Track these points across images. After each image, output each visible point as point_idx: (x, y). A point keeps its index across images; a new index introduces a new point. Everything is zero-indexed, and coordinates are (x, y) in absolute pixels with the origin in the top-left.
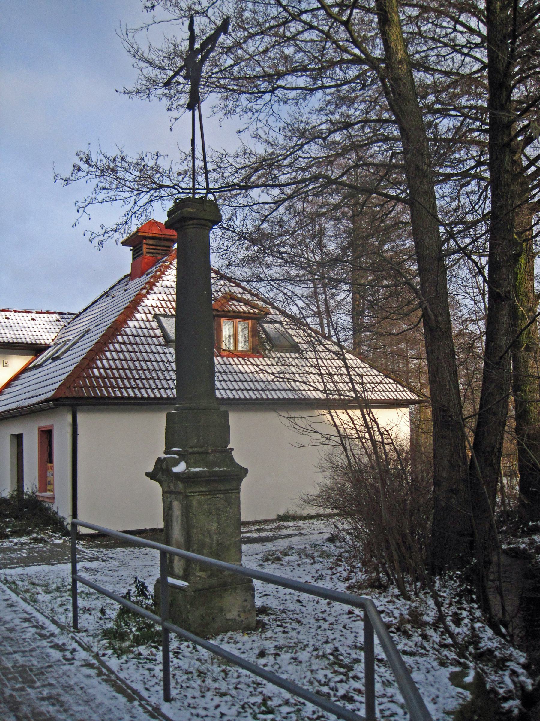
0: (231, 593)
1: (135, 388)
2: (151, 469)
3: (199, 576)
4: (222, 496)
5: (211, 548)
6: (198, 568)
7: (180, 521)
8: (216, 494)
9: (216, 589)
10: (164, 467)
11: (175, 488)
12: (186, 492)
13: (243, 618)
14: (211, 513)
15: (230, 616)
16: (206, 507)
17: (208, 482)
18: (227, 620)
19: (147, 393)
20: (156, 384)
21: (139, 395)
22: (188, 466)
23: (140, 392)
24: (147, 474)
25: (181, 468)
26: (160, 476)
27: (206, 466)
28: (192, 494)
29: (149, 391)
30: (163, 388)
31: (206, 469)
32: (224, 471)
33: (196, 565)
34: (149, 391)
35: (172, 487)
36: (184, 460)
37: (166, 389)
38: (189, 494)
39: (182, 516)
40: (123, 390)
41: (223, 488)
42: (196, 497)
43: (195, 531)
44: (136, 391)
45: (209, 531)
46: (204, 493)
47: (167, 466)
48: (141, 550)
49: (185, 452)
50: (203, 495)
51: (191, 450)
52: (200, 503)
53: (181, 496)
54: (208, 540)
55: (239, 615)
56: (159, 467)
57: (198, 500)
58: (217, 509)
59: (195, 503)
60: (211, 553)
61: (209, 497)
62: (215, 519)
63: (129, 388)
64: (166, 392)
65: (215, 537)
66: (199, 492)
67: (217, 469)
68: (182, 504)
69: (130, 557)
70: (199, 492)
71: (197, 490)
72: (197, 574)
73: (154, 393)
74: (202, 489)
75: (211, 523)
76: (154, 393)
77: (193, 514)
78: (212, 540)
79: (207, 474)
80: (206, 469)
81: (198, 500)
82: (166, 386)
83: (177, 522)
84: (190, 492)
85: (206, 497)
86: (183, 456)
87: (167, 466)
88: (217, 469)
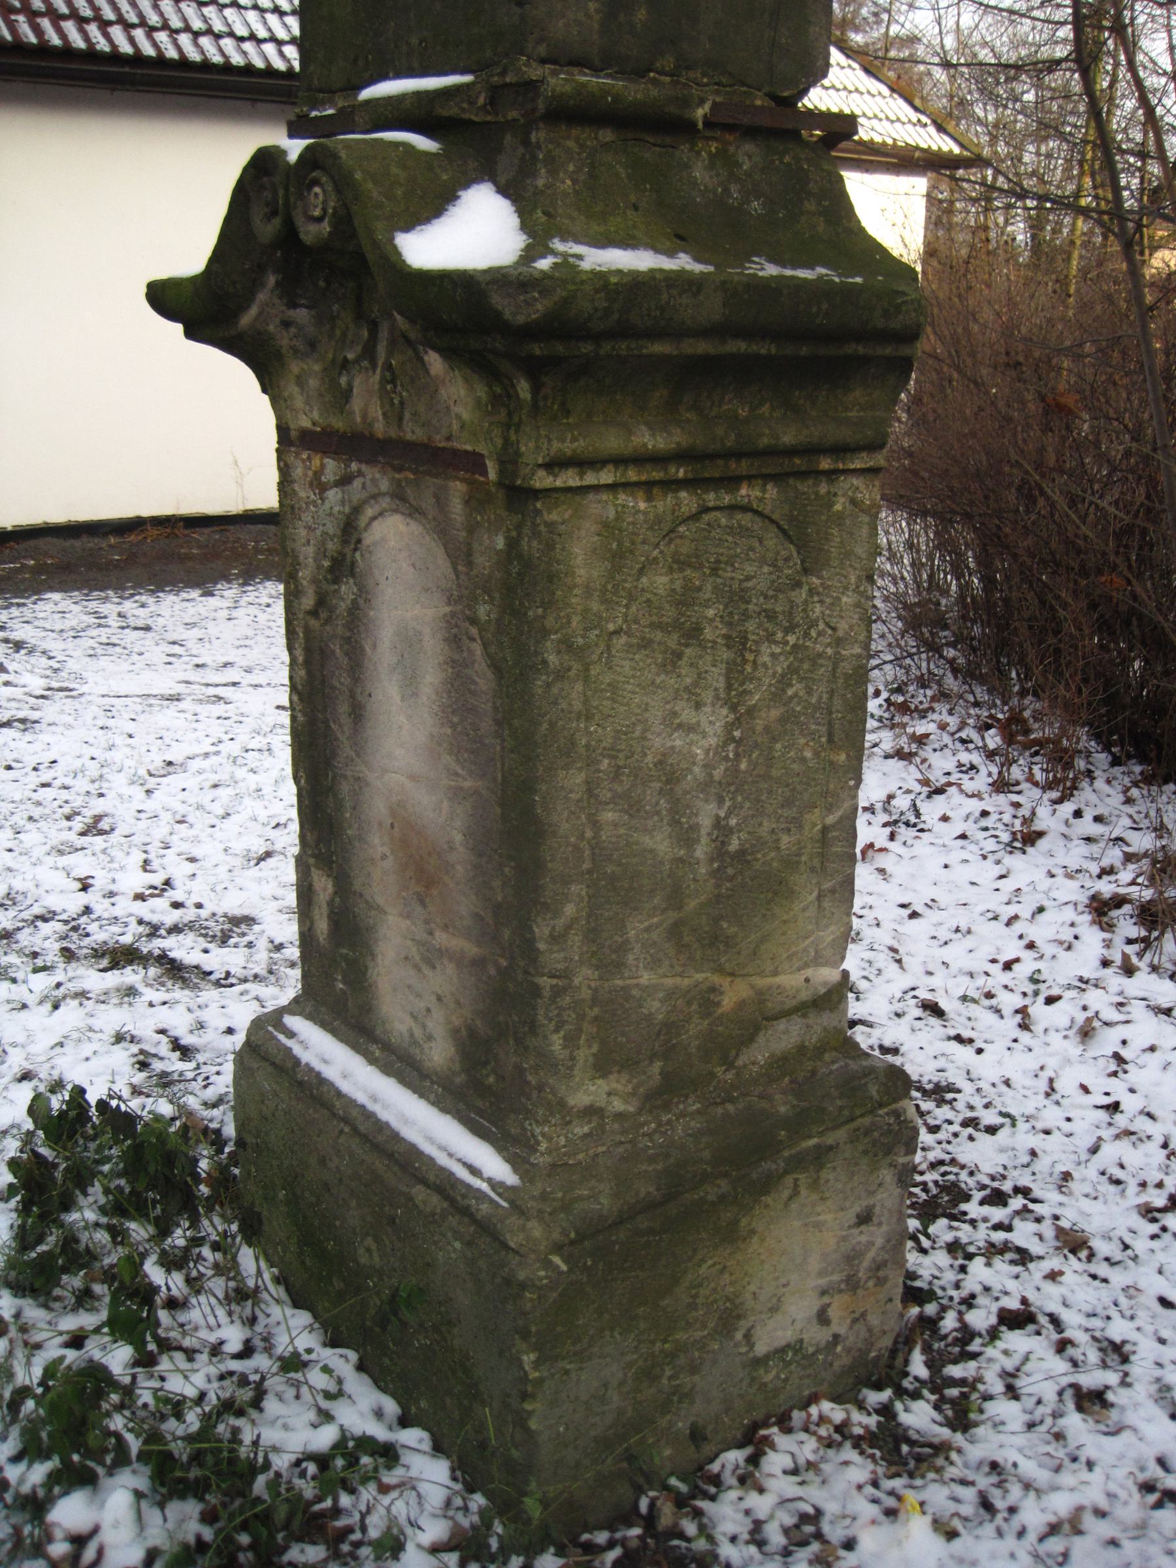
0: (796, 1193)
1: (86, 20)
2: (190, 252)
3: (591, 1111)
4: (772, 491)
5: (676, 898)
6: (585, 1054)
7: (431, 678)
8: (731, 482)
9: (711, 1192)
10: (312, 232)
11: (396, 415)
12: (509, 460)
13: (839, 1325)
14: (693, 634)
15: (770, 1335)
16: (660, 582)
17: (694, 377)
18: (760, 1362)
19: (132, 41)
20: (161, 14)
21: (103, 45)
22: (538, 223)
23: (107, 36)
24: (164, 297)
25: (474, 234)
26: (261, 309)
27: (678, 241)
28: (569, 478)
29: (139, 34)
30: (187, 29)
31: (683, 262)
32: (820, 289)
33: (571, 1041)
34: (139, 34)
35: (367, 406)
36: (486, 172)
37: (196, 35)
38: (543, 480)
39: (454, 641)
40: (45, 23)
41: (788, 437)
42: (602, 507)
43: (574, 779)
44: (93, 29)
45: (669, 774)
46: (652, 472)
47: (344, 222)
48: (128, 606)
49: (496, 94)
50: (648, 487)
51: (560, 82)
52: (617, 551)
53: (457, 489)
54: (660, 842)
55: (823, 1318)
56: (267, 230)
57: (608, 528)
58: (736, 597)
59: (581, 558)
60: (675, 931)
61: (687, 501)
62: (717, 678)
63: (64, 17)
64: (196, 45)
65: (706, 814)
66: (620, 461)
67: (772, 270)
68: (461, 555)
69: (85, 643)
70: (620, 461)
71: (612, 442)
72: (579, 1100)
73: (155, 45)
74: (648, 439)
75: (687, 714)
76: (155, 45)
77: (567, 645)
78: (687, 837)
79: (712, 309)
80: (683, 262)
81: (608, 528)
82: (197, 25)
83: (410, 684)
84: (554, 465)
85: (664, 504)
86: (473, 143)
87: (344, 222)
88: (772, 270)
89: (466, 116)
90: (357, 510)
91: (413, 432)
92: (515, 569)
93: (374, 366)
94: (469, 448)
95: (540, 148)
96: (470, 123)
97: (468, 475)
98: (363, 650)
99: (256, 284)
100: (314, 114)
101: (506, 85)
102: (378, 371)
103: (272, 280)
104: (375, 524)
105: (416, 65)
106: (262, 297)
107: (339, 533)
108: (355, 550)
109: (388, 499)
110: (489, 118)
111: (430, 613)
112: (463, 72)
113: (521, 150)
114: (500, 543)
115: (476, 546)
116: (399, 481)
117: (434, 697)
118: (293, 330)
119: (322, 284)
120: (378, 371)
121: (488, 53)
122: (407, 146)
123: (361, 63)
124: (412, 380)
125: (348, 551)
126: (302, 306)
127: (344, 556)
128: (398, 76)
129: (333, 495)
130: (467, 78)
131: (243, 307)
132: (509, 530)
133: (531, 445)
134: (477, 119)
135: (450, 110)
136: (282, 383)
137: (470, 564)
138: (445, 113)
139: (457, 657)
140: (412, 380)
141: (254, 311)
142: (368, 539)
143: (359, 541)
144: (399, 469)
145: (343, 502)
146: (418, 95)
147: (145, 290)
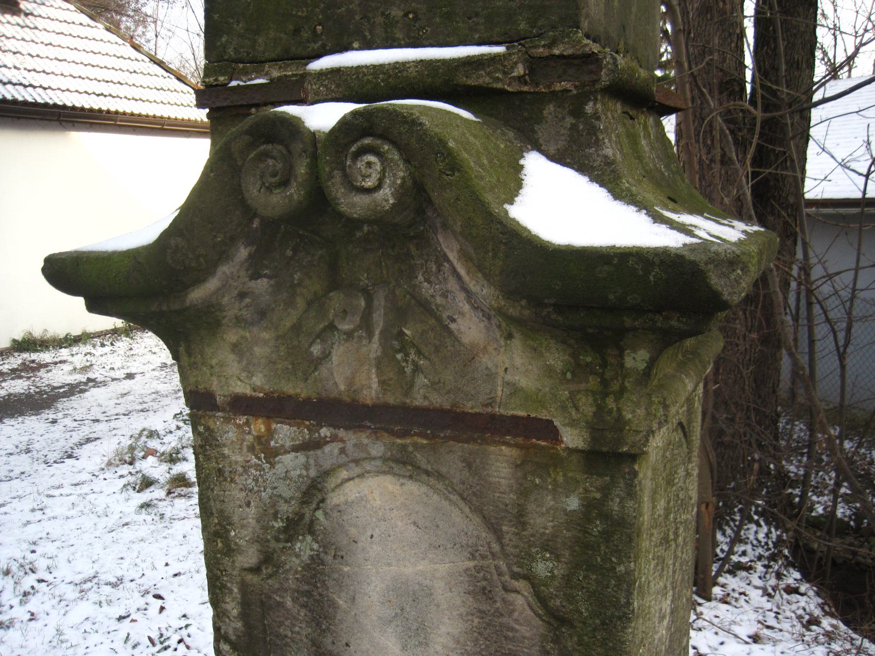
89: (499, 85)
90: (326, 474)
91: (421, 396)
92: (597, 527)
93: (370, 335)
94: (522, 413)
95: (598, 118)
96: (503, 92)
97: (520, 440)
98: (333, 604)
99: (223, 255)
100: (234, 83)
101: (553, 57)
102: (376, 337)
103: (243, 253)
104: (348, 484)
105: (400, 35)
106: (225, 269)
107: (298, 495)
108: (318, 508)
109: (379, 463)
110: (526, 89)
111: (443, 569)
112: (498, 43)
113: (569, 121)
114: (573, 503)
115: (531, 507)
116: (404, 447)
117: (452, 645)
118: (247, 300)
119: (289, 253)
120: (376, 337)
121: (523, 26)
122: (457, 116)
123: (305, 35)
124: (437, 349)
125: (307, 512)
126: (265, 276)
127: (302, 516)
128: (368, 45)
129: (289, 461)
130: (500, 49)
131: (199, 280)
132: (586, 491)
133: (641, 412)
134: (509, 89)
135: (482, 79)
136: (208, 351)
137: (523, 525)
138: (472, 82)
139: (485, 607)
140: (437, 349)
141: (212, 284)
142: (335, 499)
143: (323, 501)
144: (403, 434)
145: (306, 467)
146: (422, 62)
147: (42, 264)
